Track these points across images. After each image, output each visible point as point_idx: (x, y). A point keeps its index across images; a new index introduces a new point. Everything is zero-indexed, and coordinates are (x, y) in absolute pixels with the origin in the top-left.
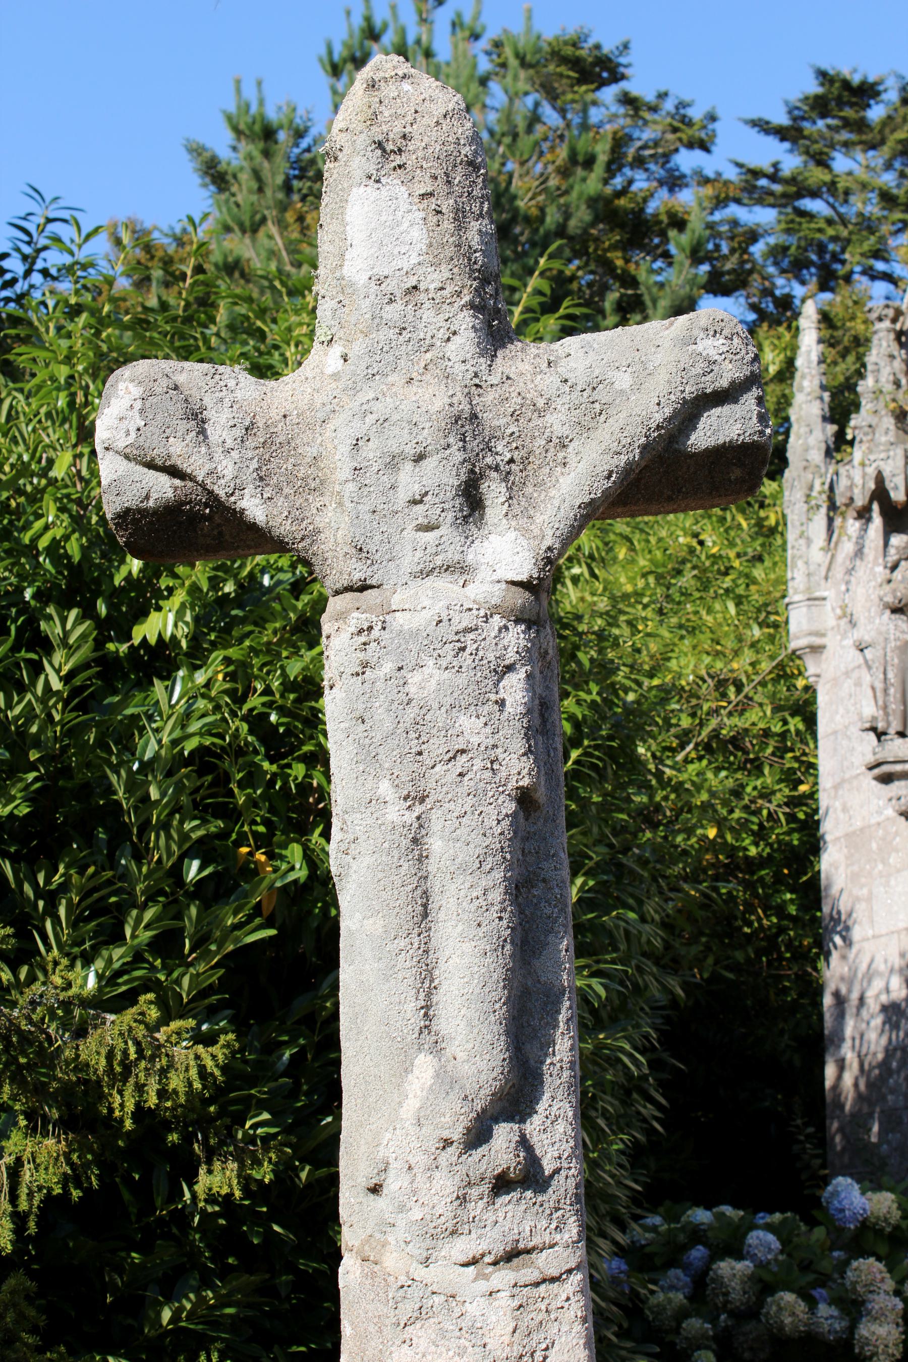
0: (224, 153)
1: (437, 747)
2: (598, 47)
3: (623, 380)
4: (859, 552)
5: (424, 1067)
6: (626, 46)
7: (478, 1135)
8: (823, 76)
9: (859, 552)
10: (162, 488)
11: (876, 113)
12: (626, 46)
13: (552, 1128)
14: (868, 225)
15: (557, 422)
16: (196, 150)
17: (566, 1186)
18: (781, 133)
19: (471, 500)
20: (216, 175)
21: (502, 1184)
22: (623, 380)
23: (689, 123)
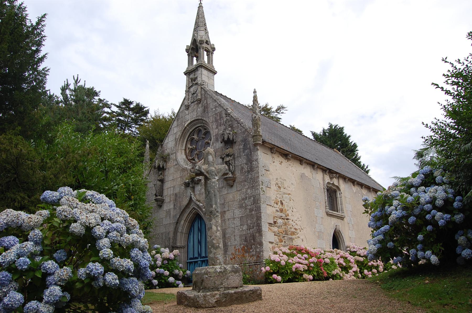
6: (100, 92)
11: (132, 106)
18: (117, 106)
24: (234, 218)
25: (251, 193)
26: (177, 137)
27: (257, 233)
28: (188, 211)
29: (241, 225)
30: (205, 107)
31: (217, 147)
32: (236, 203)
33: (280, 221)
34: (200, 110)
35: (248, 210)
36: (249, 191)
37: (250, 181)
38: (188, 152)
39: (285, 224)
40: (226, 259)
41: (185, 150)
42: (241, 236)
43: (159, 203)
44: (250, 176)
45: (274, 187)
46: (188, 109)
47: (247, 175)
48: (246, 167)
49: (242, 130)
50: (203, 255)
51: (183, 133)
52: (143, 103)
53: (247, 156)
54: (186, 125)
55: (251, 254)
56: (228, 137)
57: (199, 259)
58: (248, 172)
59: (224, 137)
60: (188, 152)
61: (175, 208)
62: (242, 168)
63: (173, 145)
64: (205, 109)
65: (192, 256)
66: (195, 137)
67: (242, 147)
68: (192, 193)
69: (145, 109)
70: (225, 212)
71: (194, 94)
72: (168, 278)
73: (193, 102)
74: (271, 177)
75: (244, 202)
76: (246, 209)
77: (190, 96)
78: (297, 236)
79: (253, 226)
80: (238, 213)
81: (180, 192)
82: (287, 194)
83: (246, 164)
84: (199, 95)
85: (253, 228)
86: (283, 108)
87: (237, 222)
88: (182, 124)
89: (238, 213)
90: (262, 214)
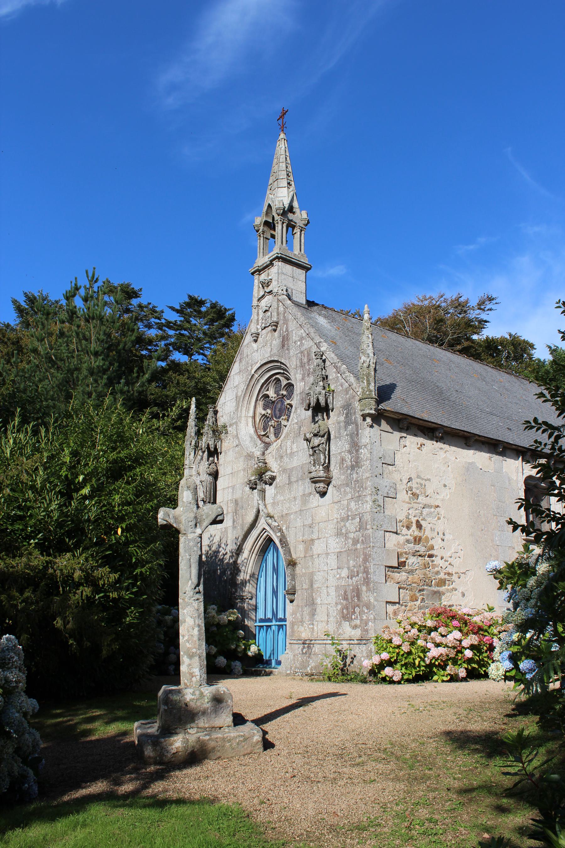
0: (23, 304)
1: (192, 550)
2: (133, 288)
3: (210, 513)
4: (202, 459)
5: (190, 582)
6: (141, 289)
7: (195, 588)
8: (190, 297)
9: (202, 459)
10: (165, 523)
11: (203, 309)
12: (141, 289)
13: (201, 588)
14: (199, 340)
15: (204, 517)
16: (15, 302)
17: (202, 593)
18: (178, 311)
19: (196, 525)
20: (20, 310)
21: (197, 593)
22: (210, 513)
23: (156, 312)
24: (327, 554)
25: (356, 509)
26: (239, 394)
27: (363, 584)
28: (255, 533)
29: (338, 568)
30: (283, 337)
31: (303, 417)
34: (276, 342)
35: (350, 541)
36: (353, 504)
37: (355, 485)
38: (257, 420)
39: (426, 566)
40: (313, 628)
41: (254, 417)
42: (337, 588)
44: (355, 476)
45: (403, 496)
46: (256, 341)
47: (351, 474)
48: (348, 457)
49: (344, 387)
50: (281, 615)
51: (248, 385)
52: (224, 303)
53: (351, 437)
54: (253, 372)
55: (353, 623)
57: (274, 623)
58: (353, 467)
59: (309, 400)
60: (257, 420)
61: (234, 527)
62: (343, 460)
63: (233, 409)
64: (285, 341)
66: (271, 393)
67: (342, 418)
69: (227, 314)
71: (266, 311)
72: (216, 658)
73: (265, 328)
75: (345, 526)
76: (347, 538)
77: (261, 316)
78: (451, 587)
79: (358, 572)
80: (335, 545)
81: (242, 498)
82: (430, 507)
83: (350, 452)
84: (275, 314)
85: (358, 575)
86: (491, 299)
87: (333, 562)
88: (246, 368)
89: (335, 545)
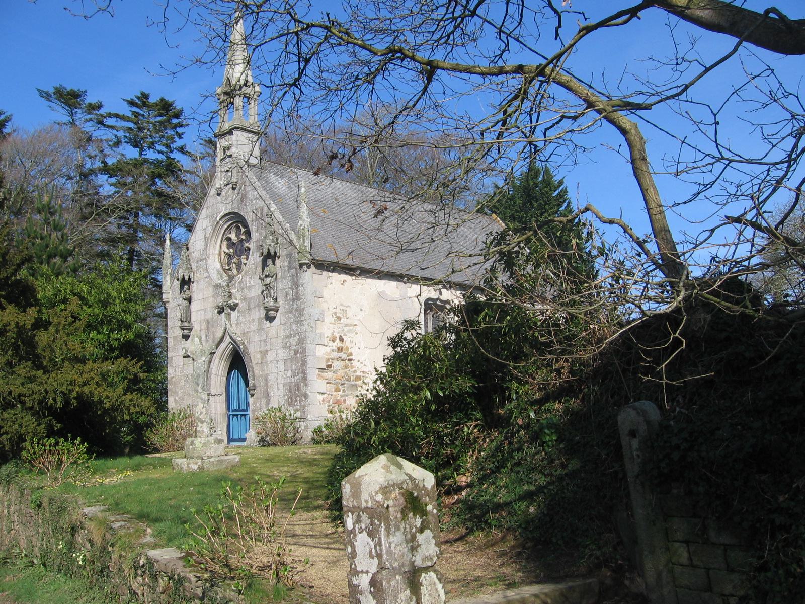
24: (277, 361)
25: (297, 330)
32: (280, 341)
33: (337, 365)
35: (293, 352)
39: (346, 367)
41: (220, 255)
42: (285, 384)
43: (186, 332)
45: (329, 319)
54: (218, 219)
56: (269, 250)
65: (236, 407)
67: (286, 264)
68: (227, 322)
70: (267, 351)
74: (325, 306)
80: (282, 354)
81: (212, 318)
82: (350, 325)
83: (292, 289)
87: (281, 366)
90: (308, 358)
